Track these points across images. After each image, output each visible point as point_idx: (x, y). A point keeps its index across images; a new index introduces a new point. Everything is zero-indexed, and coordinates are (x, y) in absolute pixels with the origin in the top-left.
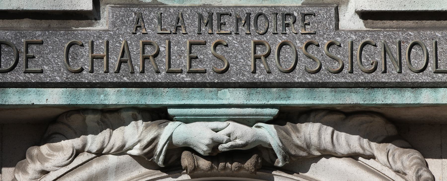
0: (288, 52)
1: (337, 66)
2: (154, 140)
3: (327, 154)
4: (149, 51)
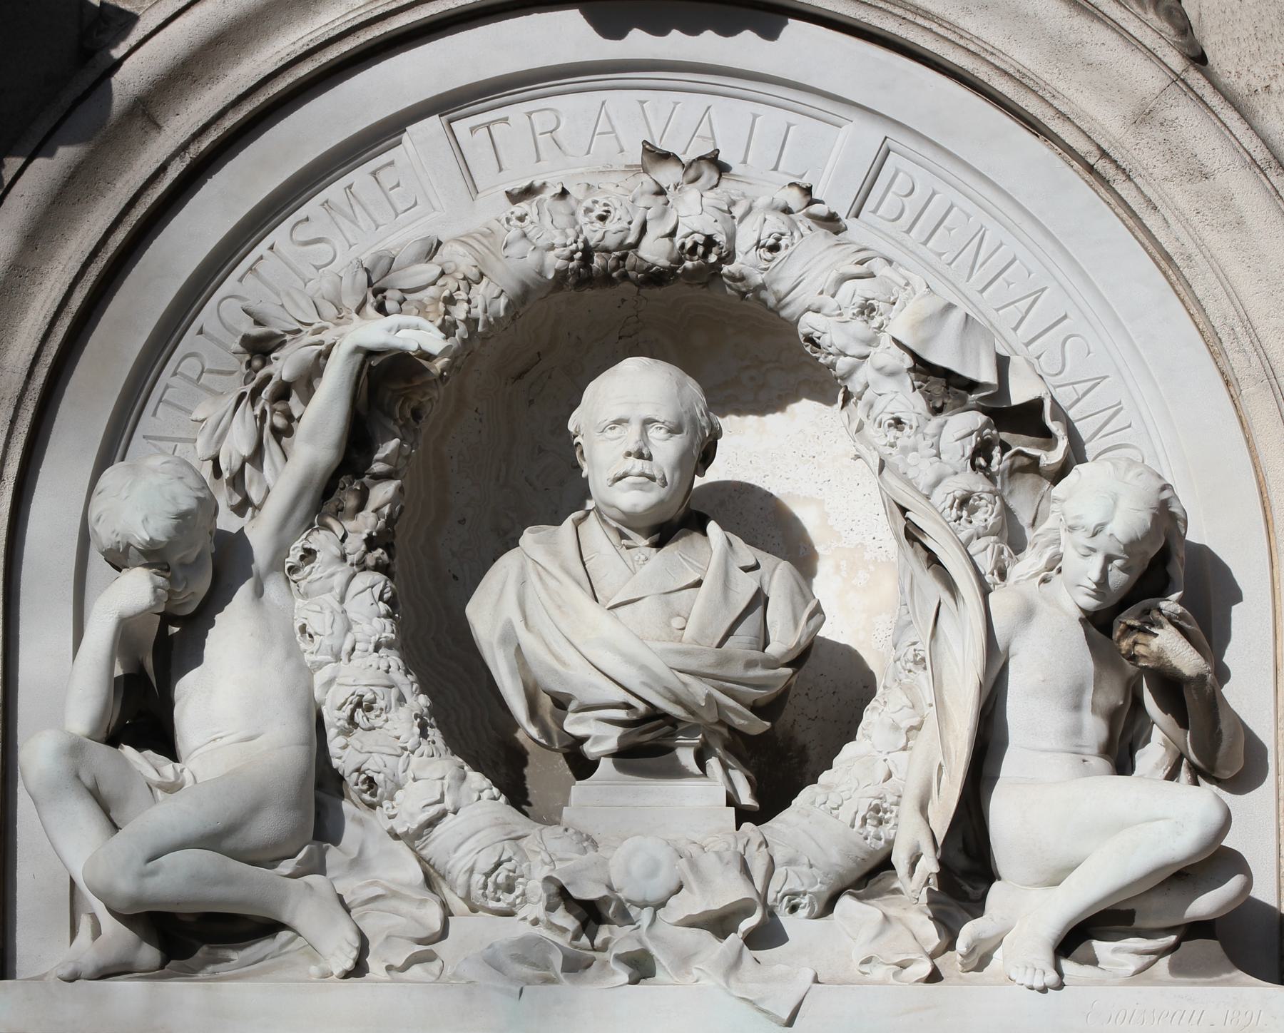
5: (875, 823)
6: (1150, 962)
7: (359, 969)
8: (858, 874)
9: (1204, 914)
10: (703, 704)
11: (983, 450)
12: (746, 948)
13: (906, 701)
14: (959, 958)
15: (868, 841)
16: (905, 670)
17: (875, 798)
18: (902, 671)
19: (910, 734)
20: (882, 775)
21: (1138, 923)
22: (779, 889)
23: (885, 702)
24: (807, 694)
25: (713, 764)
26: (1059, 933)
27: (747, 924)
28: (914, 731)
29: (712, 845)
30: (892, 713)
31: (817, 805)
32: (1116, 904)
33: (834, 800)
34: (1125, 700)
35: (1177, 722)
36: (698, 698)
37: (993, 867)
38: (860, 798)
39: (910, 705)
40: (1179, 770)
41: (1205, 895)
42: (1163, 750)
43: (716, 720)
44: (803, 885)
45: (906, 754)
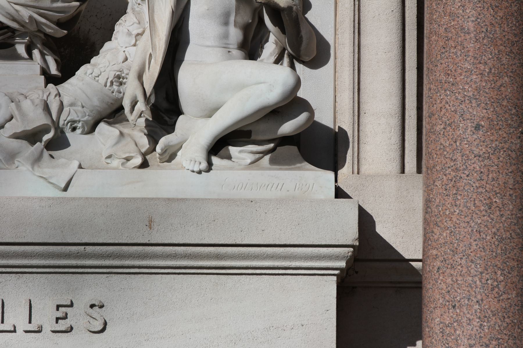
5: (118, 84)
6: (259, 158)
8: (109, 111)
9: (287, 132)
10: (27, 21)
12: (45, 150)
13: (136, 20)
14: (158, 155)
15: (114, 94)
16: (137, 4)
17: (118, 71)
18: (135, 4)
19: (138, 37)
20: (121, 58)
21: (253, 137)
22: (65, 119)
23: (125, 21)
24: (96, 16)
25: (36, 53)
26: (210, 142)
27: (47, 137)
28: (140, 36)
29: (31, 95)
30: (128, 26)
31: (88, 75)
32: (241, 127)
33: (96, 72)
34: (253, 19)
35: (281, 30)
36: (25, 18)
37: (180, 107)
38: (110, 71)
39: (137, 22)
40: (283, 56)
41: (287, 123)
42: (274, 46)
43: (36, 30)
44: (78, 117)
45: (135, 48)
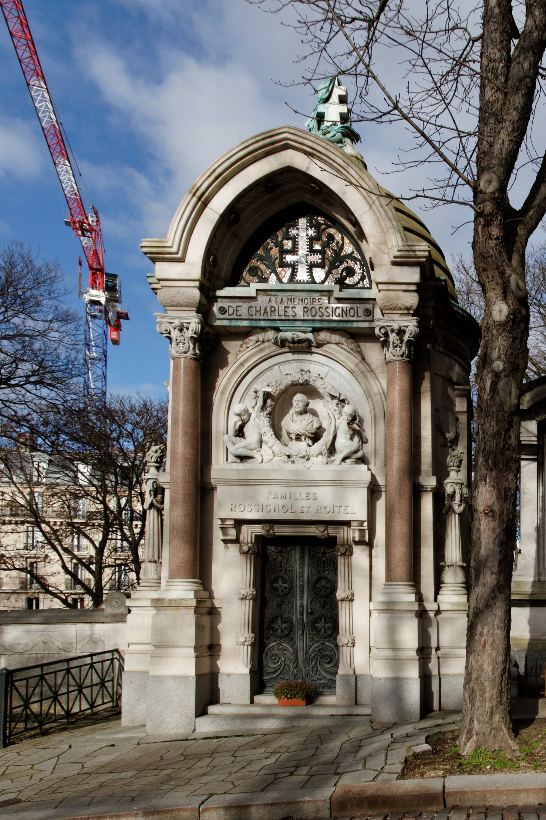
0: (314, 310)
1: (328, 315)
2: (277, 337)
3: (328, 343)
4: (273, 309)
7: (262, 462)
11: (338, 404)
